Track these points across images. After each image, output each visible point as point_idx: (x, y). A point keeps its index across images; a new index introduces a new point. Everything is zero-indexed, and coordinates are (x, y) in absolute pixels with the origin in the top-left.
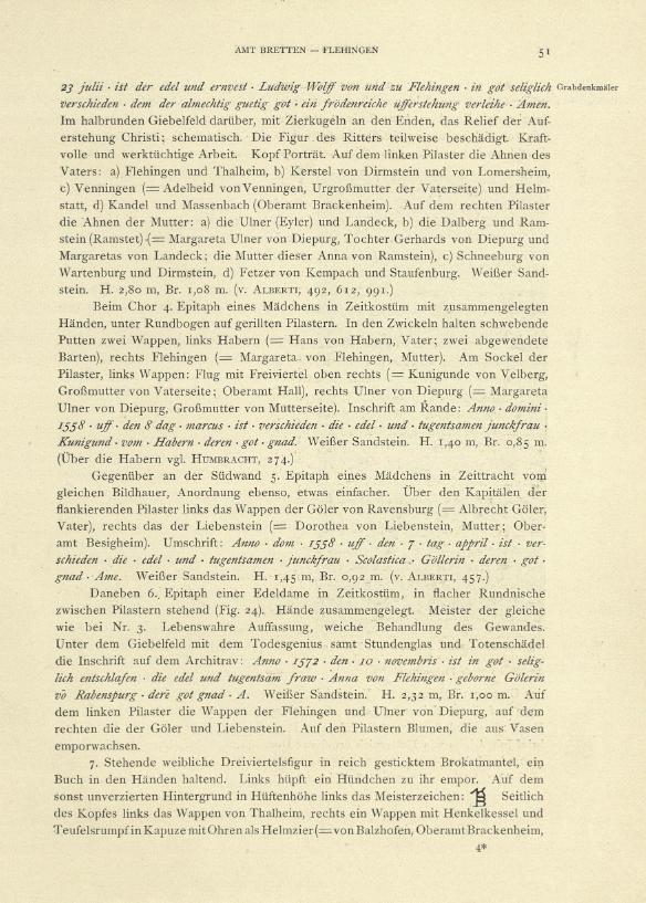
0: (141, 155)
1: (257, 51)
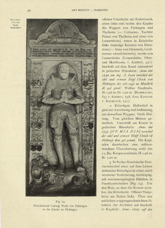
0: (121, 192)
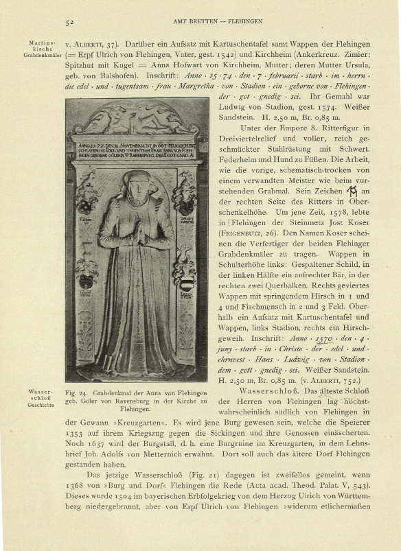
1: (188, 22)
